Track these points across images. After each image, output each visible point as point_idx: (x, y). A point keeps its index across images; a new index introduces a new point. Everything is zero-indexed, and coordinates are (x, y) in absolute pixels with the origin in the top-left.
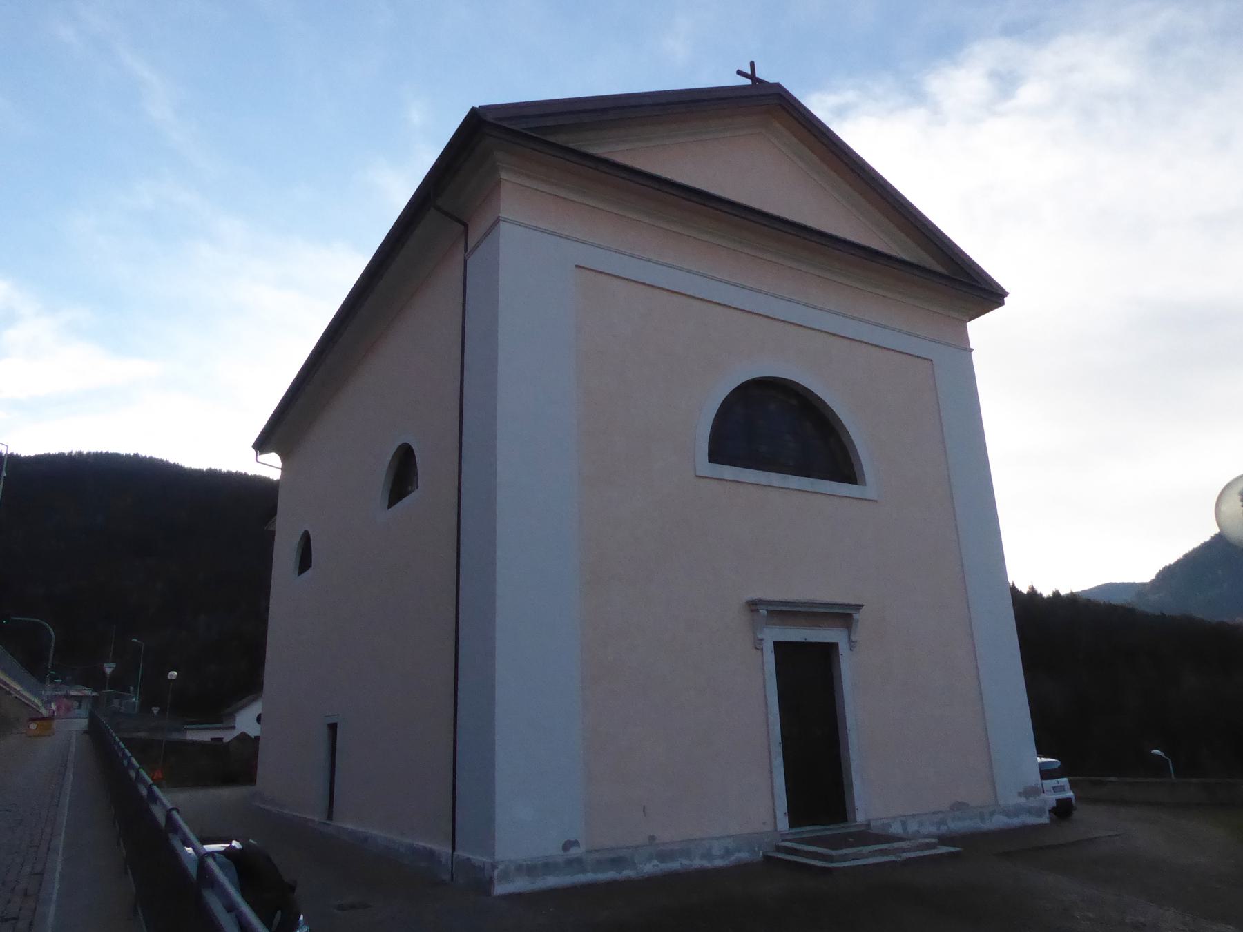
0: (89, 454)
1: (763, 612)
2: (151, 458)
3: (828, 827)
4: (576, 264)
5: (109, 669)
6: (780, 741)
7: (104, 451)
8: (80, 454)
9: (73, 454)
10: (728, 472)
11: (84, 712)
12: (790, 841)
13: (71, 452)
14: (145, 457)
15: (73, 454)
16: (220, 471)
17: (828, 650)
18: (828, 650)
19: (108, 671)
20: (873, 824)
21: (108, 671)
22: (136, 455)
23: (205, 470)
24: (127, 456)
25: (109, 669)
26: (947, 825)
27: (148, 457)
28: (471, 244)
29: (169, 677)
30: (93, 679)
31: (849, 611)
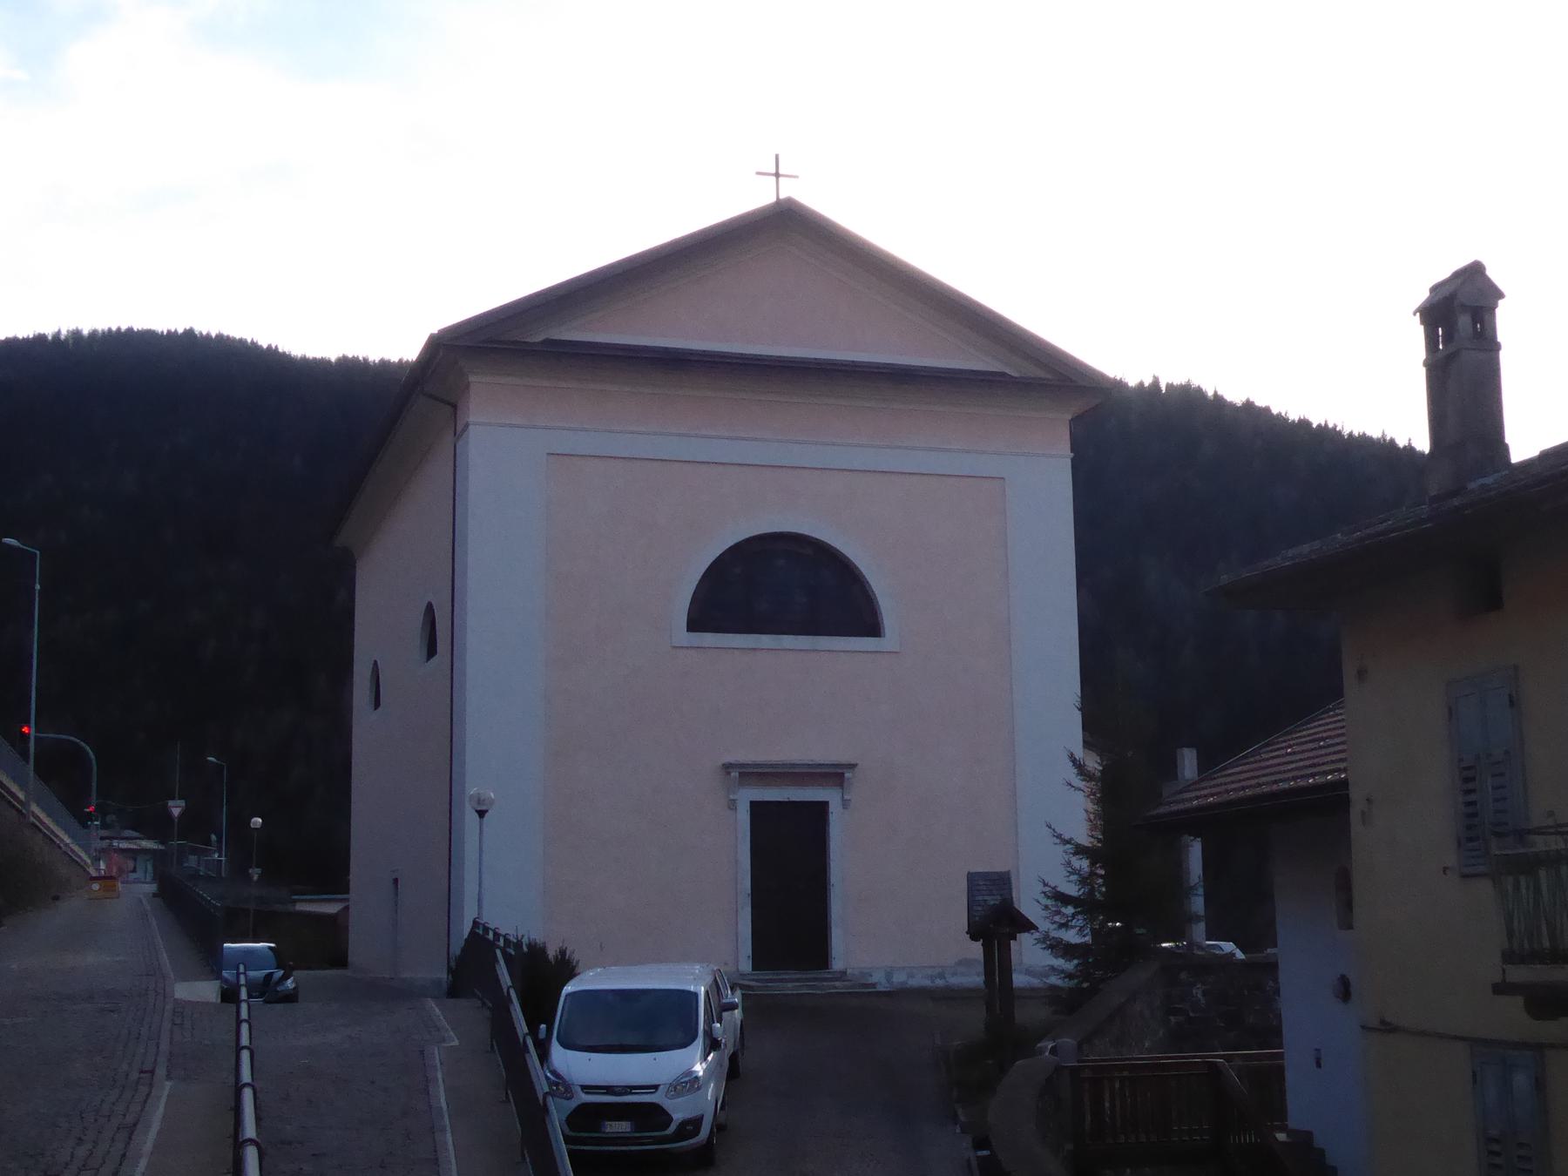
0: (94, 334)
1: (735, 774)
2: (220, 337)
3: (804, 976)
4: (548, 451)
5: (176, 808)
6: (750, 892)
7: (124, 328)
8: (76, 335)
9: (62, 337)
10: (709, 639)
11: (146, 869)
12: (753, 980)
13: (59, 332)
14: (208, 335)
15: (62, 337)
16: (365, 360)
17: (821, 809)
18: (821, 809)
19: (176, 812)
20: (849, 971)
21: (176, 812)
22: (189, 333)
23: (333, 359)
24: (172, 336)
25: (176, 808)
26: (945, 978)
27: (213, 335)
28: (459, 429)
29: (252, 826)
30: (156, 825)
31: (840, 771)
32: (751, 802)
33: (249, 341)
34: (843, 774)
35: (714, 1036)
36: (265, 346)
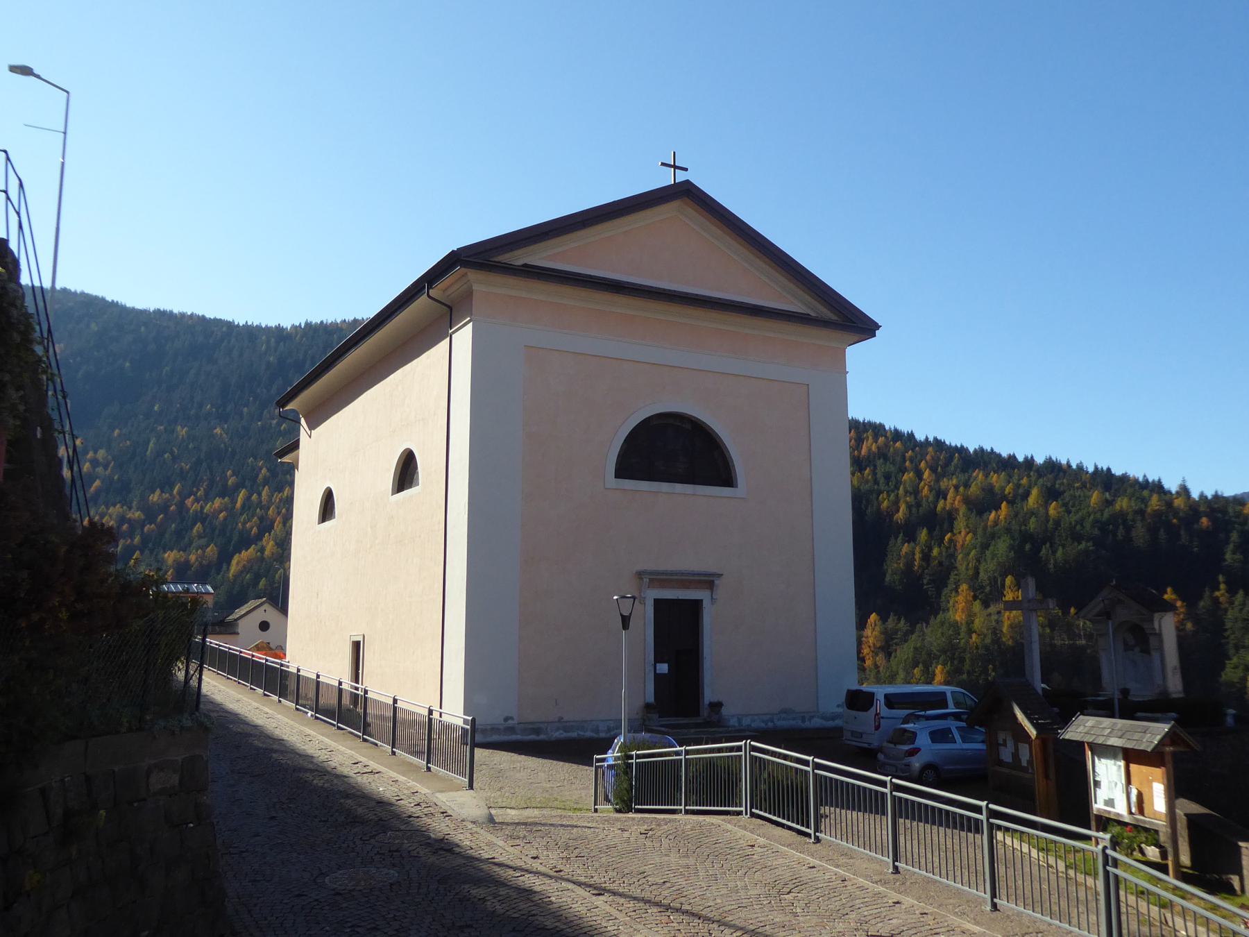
1: (646, 580)
17: (696, 605)
18: (696, 605)
31: (712, 579)
32: (654, 599)
33: (989, 450)
34: (713, 581)
35: (1001, 758)
36: (110, 301)
